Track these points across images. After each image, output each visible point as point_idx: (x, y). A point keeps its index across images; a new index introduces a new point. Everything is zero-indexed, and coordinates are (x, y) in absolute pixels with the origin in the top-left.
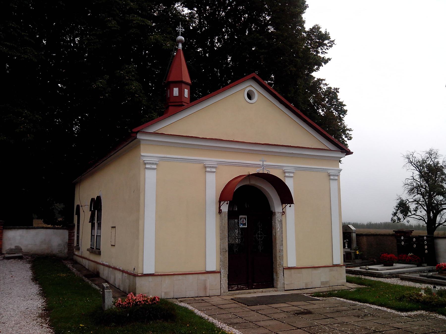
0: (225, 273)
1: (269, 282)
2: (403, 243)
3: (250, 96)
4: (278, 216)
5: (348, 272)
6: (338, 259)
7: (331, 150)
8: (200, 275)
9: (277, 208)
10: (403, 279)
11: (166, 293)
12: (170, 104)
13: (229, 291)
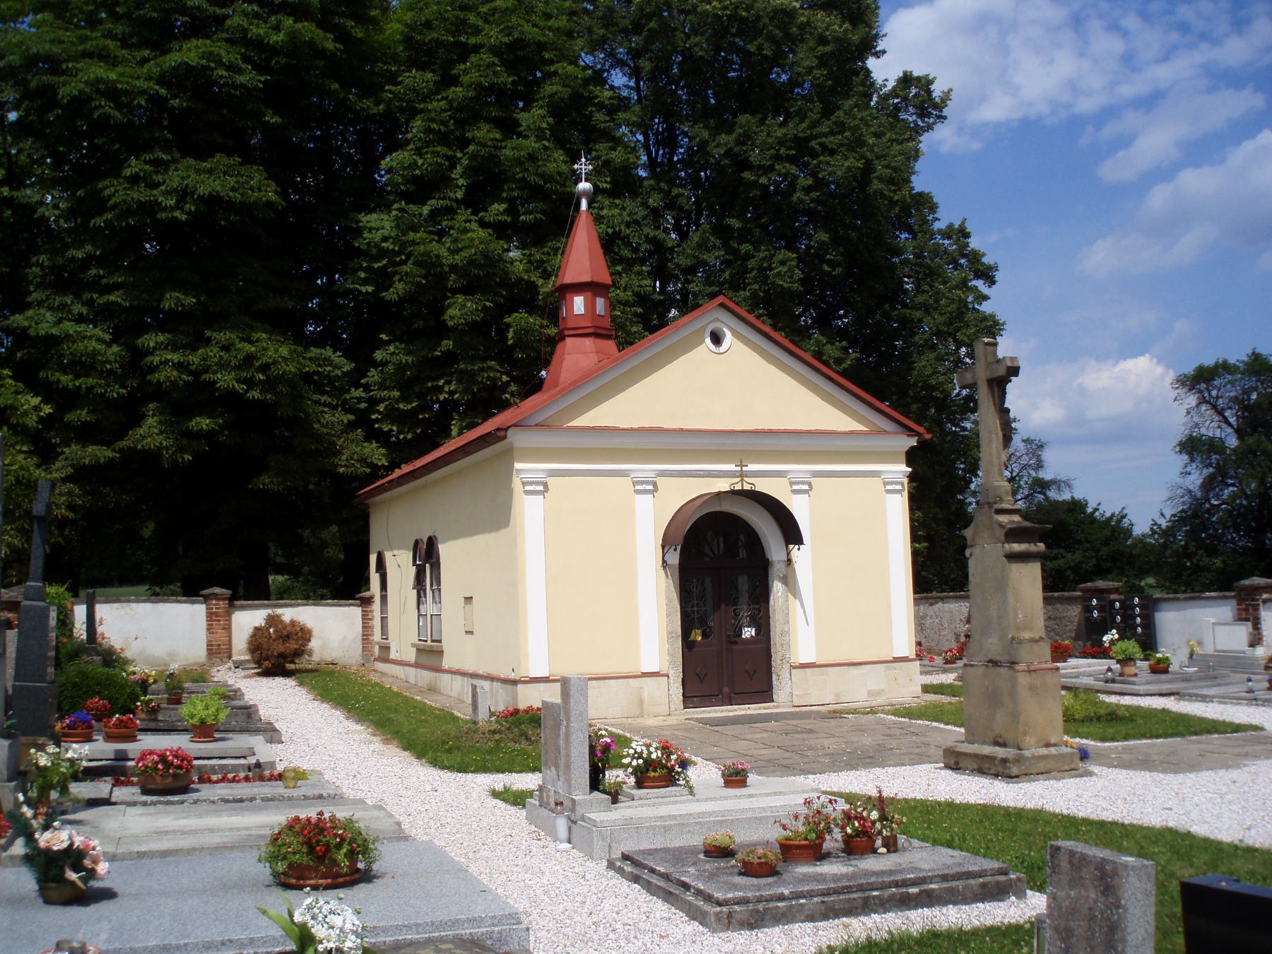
1: (764, 692)
2: (1096, 614)
3: (717, 339)
6: (904, 644)
7: (885, 432)
8: (631, 680)
12: (567, 333)
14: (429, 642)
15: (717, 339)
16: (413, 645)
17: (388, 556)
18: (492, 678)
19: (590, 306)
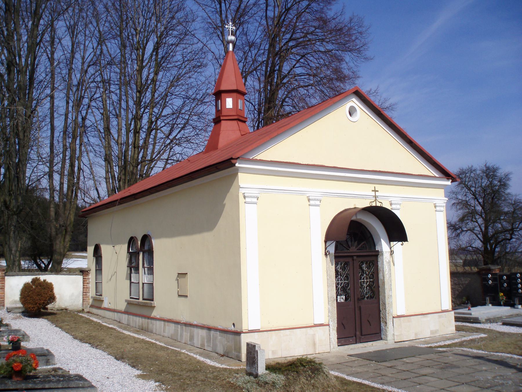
0: (334, 325)
1: (376, 332)
2: (490, 282)
4: (386, 256)
5: (457, 319)
9: (384, 246)
10: (504, 324)
11: (273, 352)
12: (222, 118)
13: (338, 346)
14: (141, 300)
15: (352, 112)
16: (126, 301)
17: (105, 249)
18: (202, 327)
19: (235, 103)
